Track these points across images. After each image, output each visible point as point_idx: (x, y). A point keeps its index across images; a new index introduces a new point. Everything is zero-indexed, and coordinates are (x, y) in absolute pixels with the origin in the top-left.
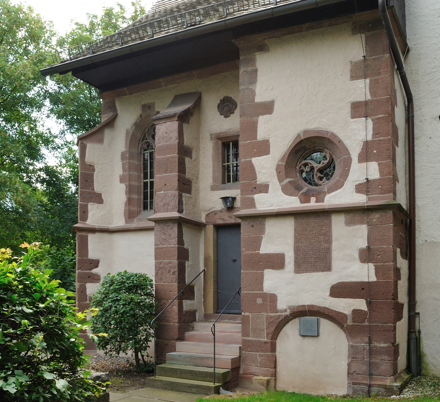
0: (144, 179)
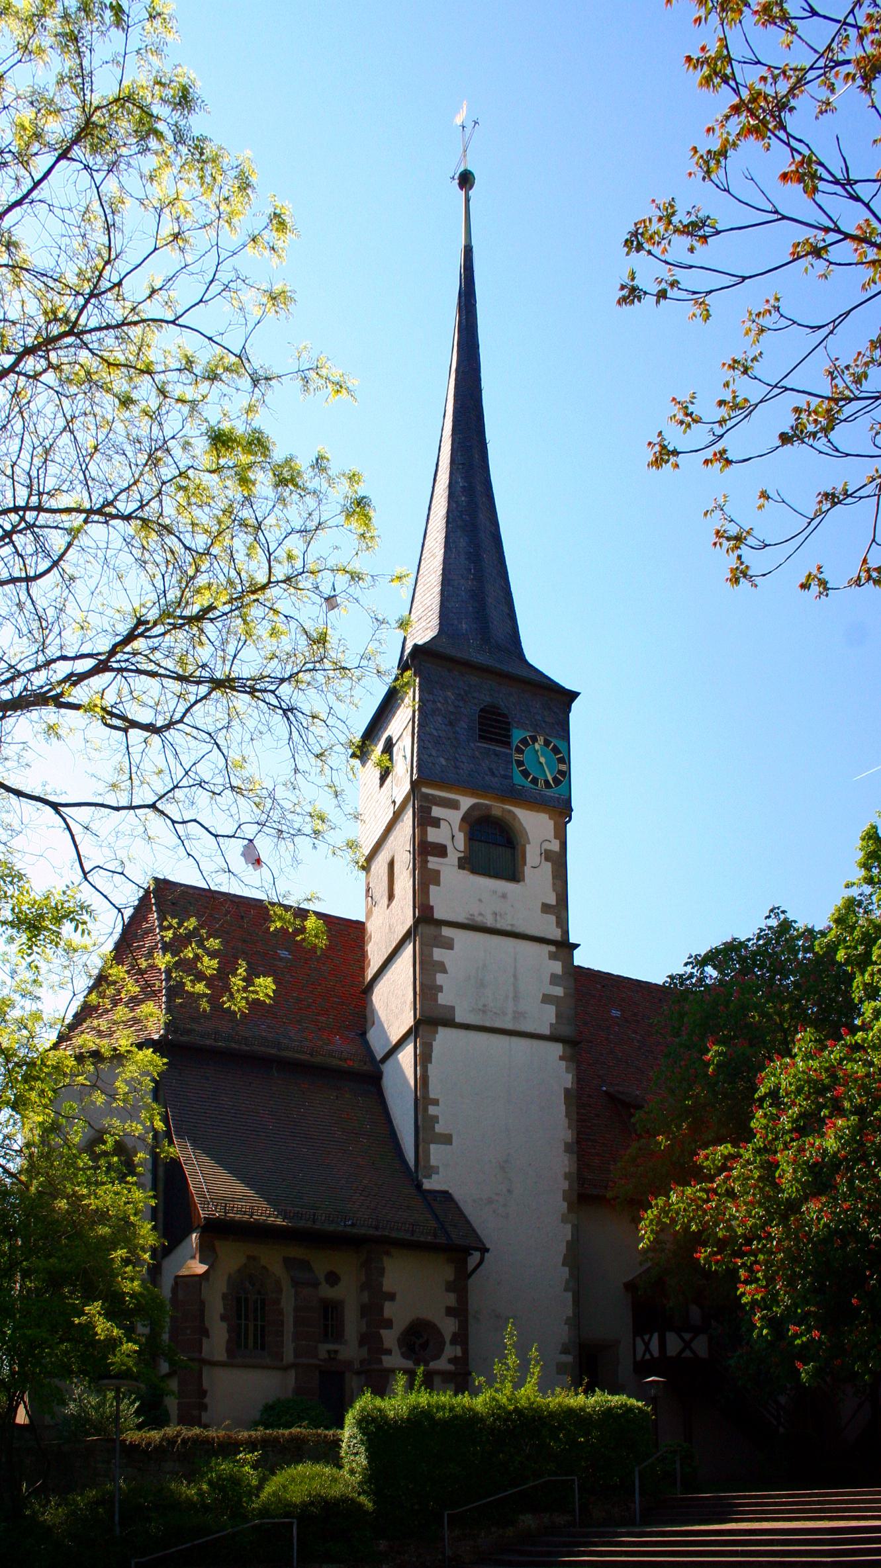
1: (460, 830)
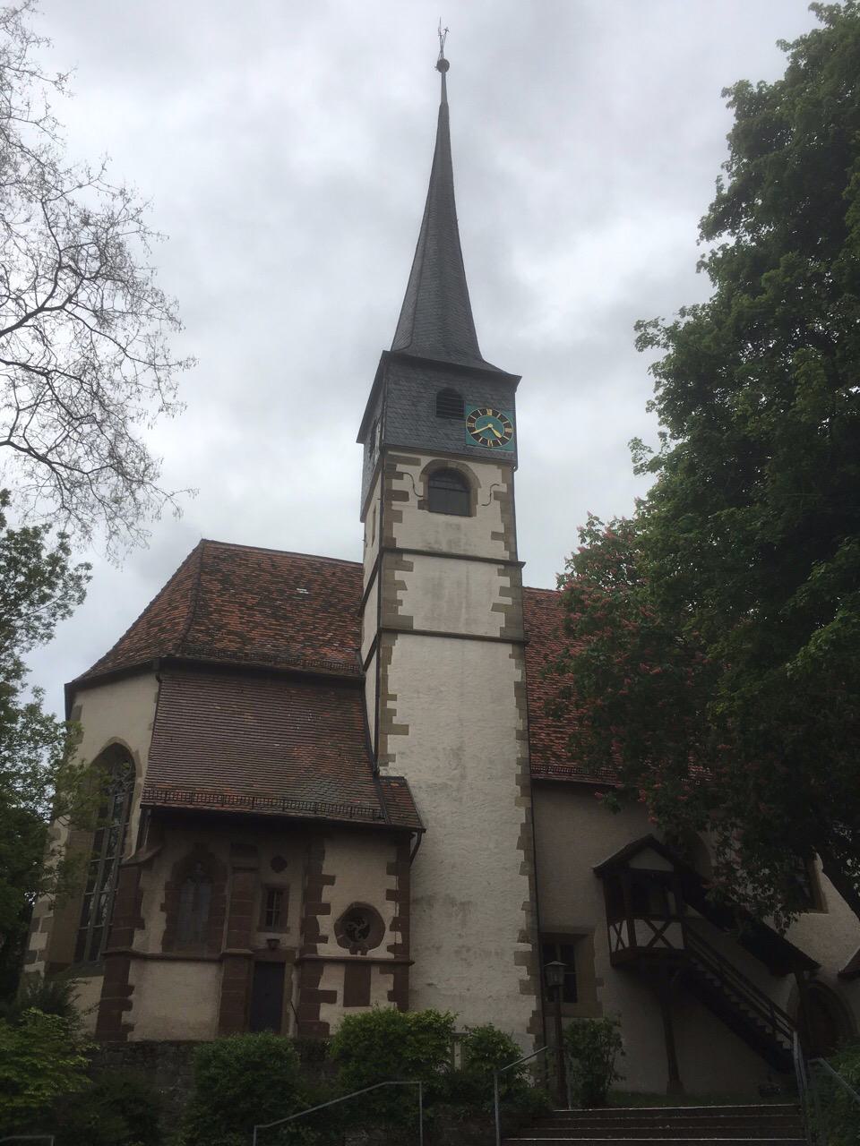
0: (88, 891)
1: (420, 480)
